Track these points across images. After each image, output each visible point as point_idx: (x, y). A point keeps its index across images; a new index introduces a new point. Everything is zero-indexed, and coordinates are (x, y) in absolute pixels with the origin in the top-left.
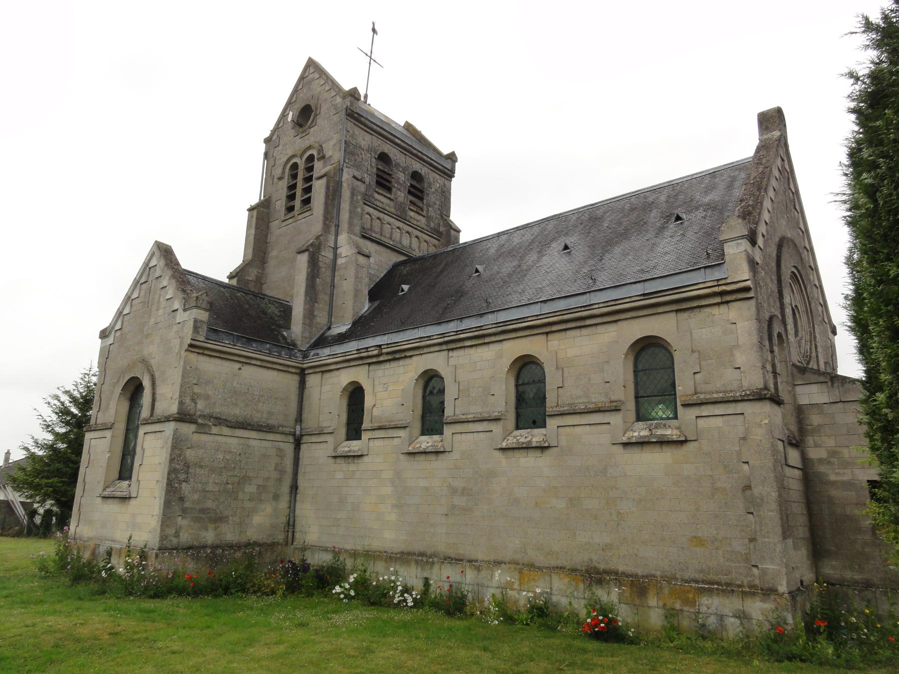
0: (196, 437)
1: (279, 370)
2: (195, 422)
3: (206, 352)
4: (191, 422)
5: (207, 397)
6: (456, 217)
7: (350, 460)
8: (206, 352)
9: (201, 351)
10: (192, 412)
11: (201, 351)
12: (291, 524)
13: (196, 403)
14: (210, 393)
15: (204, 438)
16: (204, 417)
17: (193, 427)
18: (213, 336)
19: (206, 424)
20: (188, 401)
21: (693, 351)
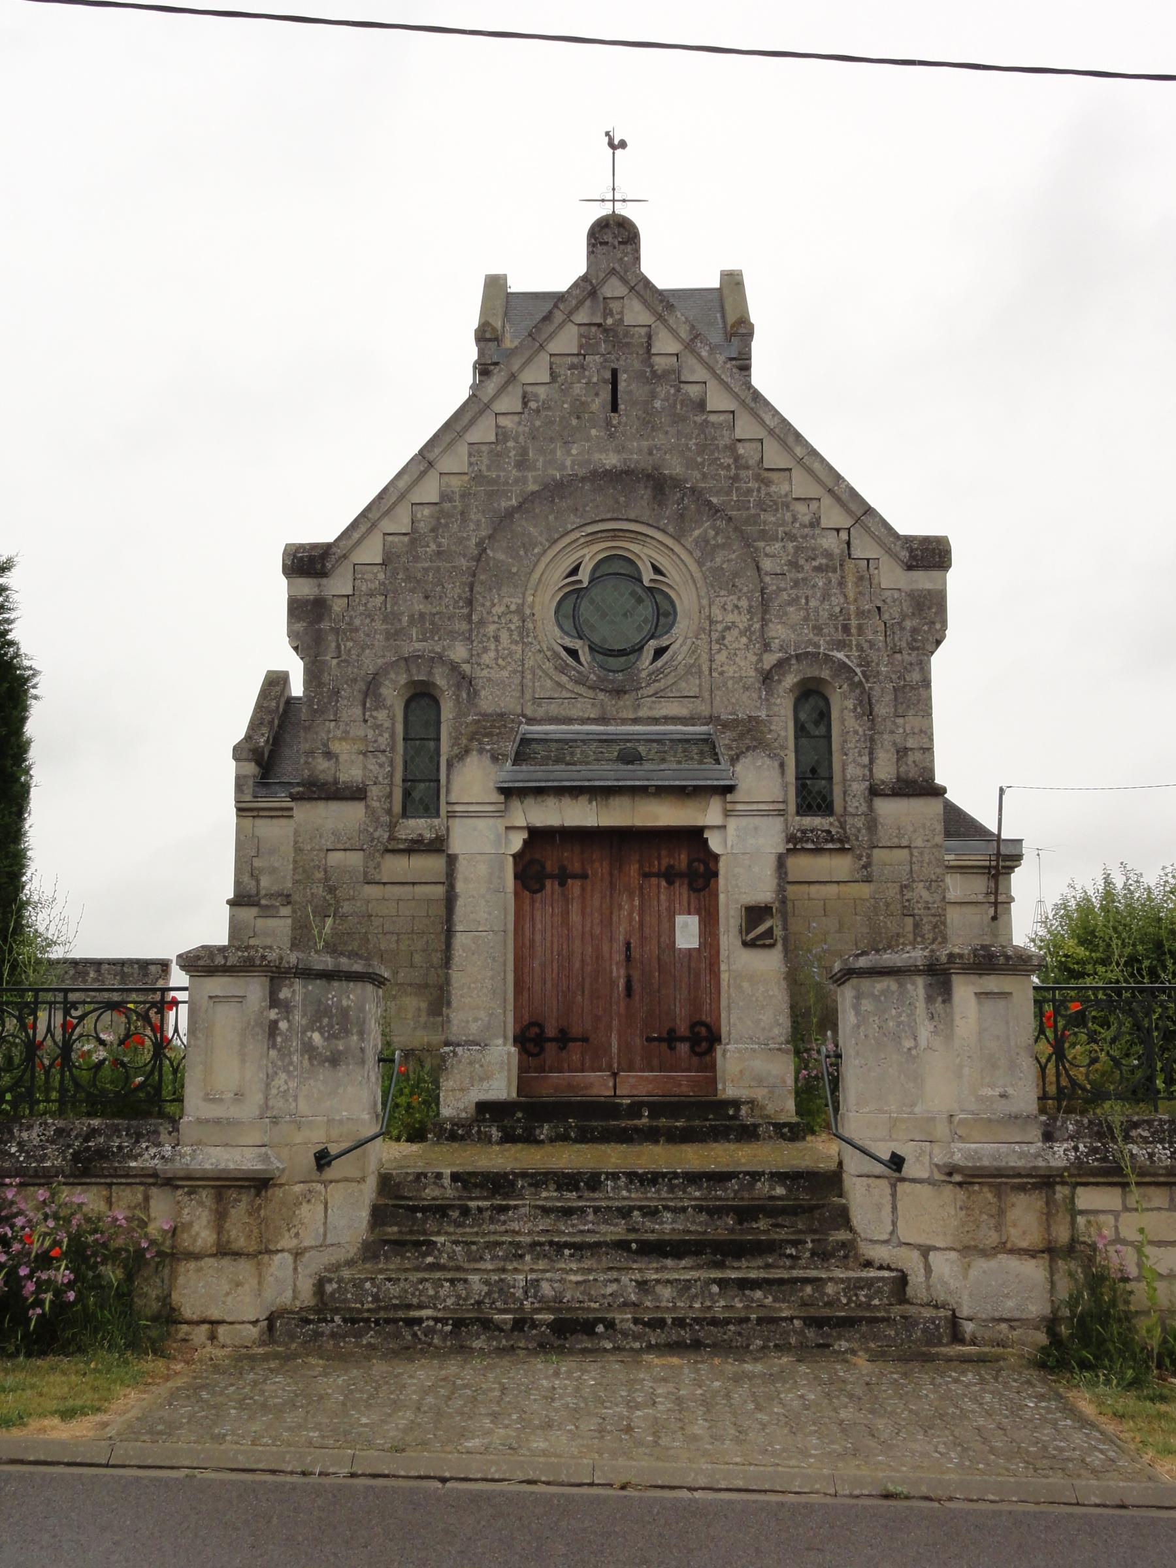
0: (260, 923)
1: (272, 817)
2: (256, 904)
3: (261, 814)
4: (253, 905)
5: (273, 871)
6: (562, 284)
7: (224, 1176)
8: (261, 814)
9: (255, 814)
10: (254, 891)
11: (255, 814)
12: (196, 1257)
13: (258, 881)
14: (276, 864)
15: (272, 923)
16: (270, 896)
17: (254, 911)
18: (263, 792)
19: (272, 906)
20: (246, 879)
21: (921, 731)
